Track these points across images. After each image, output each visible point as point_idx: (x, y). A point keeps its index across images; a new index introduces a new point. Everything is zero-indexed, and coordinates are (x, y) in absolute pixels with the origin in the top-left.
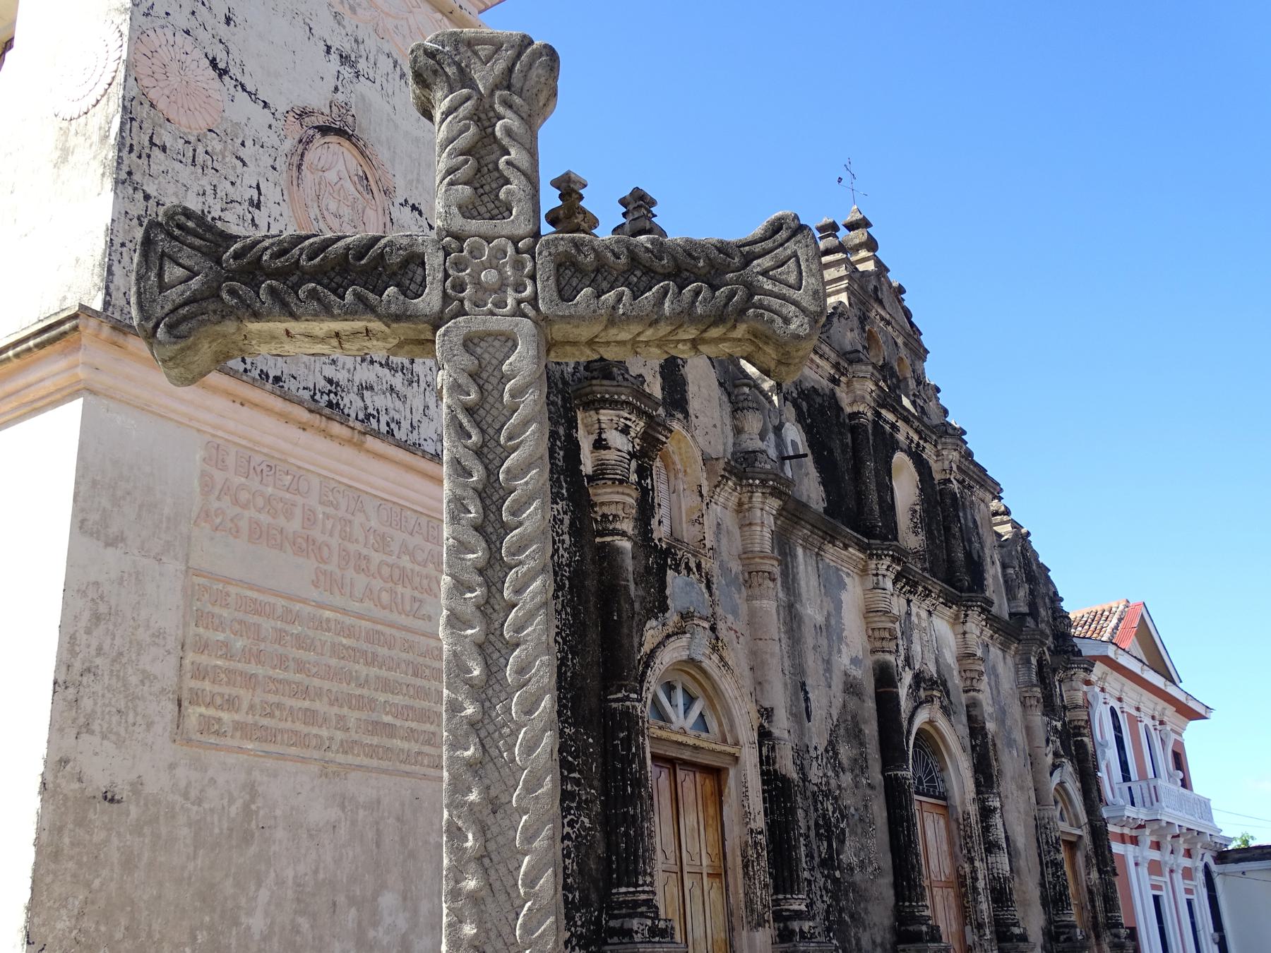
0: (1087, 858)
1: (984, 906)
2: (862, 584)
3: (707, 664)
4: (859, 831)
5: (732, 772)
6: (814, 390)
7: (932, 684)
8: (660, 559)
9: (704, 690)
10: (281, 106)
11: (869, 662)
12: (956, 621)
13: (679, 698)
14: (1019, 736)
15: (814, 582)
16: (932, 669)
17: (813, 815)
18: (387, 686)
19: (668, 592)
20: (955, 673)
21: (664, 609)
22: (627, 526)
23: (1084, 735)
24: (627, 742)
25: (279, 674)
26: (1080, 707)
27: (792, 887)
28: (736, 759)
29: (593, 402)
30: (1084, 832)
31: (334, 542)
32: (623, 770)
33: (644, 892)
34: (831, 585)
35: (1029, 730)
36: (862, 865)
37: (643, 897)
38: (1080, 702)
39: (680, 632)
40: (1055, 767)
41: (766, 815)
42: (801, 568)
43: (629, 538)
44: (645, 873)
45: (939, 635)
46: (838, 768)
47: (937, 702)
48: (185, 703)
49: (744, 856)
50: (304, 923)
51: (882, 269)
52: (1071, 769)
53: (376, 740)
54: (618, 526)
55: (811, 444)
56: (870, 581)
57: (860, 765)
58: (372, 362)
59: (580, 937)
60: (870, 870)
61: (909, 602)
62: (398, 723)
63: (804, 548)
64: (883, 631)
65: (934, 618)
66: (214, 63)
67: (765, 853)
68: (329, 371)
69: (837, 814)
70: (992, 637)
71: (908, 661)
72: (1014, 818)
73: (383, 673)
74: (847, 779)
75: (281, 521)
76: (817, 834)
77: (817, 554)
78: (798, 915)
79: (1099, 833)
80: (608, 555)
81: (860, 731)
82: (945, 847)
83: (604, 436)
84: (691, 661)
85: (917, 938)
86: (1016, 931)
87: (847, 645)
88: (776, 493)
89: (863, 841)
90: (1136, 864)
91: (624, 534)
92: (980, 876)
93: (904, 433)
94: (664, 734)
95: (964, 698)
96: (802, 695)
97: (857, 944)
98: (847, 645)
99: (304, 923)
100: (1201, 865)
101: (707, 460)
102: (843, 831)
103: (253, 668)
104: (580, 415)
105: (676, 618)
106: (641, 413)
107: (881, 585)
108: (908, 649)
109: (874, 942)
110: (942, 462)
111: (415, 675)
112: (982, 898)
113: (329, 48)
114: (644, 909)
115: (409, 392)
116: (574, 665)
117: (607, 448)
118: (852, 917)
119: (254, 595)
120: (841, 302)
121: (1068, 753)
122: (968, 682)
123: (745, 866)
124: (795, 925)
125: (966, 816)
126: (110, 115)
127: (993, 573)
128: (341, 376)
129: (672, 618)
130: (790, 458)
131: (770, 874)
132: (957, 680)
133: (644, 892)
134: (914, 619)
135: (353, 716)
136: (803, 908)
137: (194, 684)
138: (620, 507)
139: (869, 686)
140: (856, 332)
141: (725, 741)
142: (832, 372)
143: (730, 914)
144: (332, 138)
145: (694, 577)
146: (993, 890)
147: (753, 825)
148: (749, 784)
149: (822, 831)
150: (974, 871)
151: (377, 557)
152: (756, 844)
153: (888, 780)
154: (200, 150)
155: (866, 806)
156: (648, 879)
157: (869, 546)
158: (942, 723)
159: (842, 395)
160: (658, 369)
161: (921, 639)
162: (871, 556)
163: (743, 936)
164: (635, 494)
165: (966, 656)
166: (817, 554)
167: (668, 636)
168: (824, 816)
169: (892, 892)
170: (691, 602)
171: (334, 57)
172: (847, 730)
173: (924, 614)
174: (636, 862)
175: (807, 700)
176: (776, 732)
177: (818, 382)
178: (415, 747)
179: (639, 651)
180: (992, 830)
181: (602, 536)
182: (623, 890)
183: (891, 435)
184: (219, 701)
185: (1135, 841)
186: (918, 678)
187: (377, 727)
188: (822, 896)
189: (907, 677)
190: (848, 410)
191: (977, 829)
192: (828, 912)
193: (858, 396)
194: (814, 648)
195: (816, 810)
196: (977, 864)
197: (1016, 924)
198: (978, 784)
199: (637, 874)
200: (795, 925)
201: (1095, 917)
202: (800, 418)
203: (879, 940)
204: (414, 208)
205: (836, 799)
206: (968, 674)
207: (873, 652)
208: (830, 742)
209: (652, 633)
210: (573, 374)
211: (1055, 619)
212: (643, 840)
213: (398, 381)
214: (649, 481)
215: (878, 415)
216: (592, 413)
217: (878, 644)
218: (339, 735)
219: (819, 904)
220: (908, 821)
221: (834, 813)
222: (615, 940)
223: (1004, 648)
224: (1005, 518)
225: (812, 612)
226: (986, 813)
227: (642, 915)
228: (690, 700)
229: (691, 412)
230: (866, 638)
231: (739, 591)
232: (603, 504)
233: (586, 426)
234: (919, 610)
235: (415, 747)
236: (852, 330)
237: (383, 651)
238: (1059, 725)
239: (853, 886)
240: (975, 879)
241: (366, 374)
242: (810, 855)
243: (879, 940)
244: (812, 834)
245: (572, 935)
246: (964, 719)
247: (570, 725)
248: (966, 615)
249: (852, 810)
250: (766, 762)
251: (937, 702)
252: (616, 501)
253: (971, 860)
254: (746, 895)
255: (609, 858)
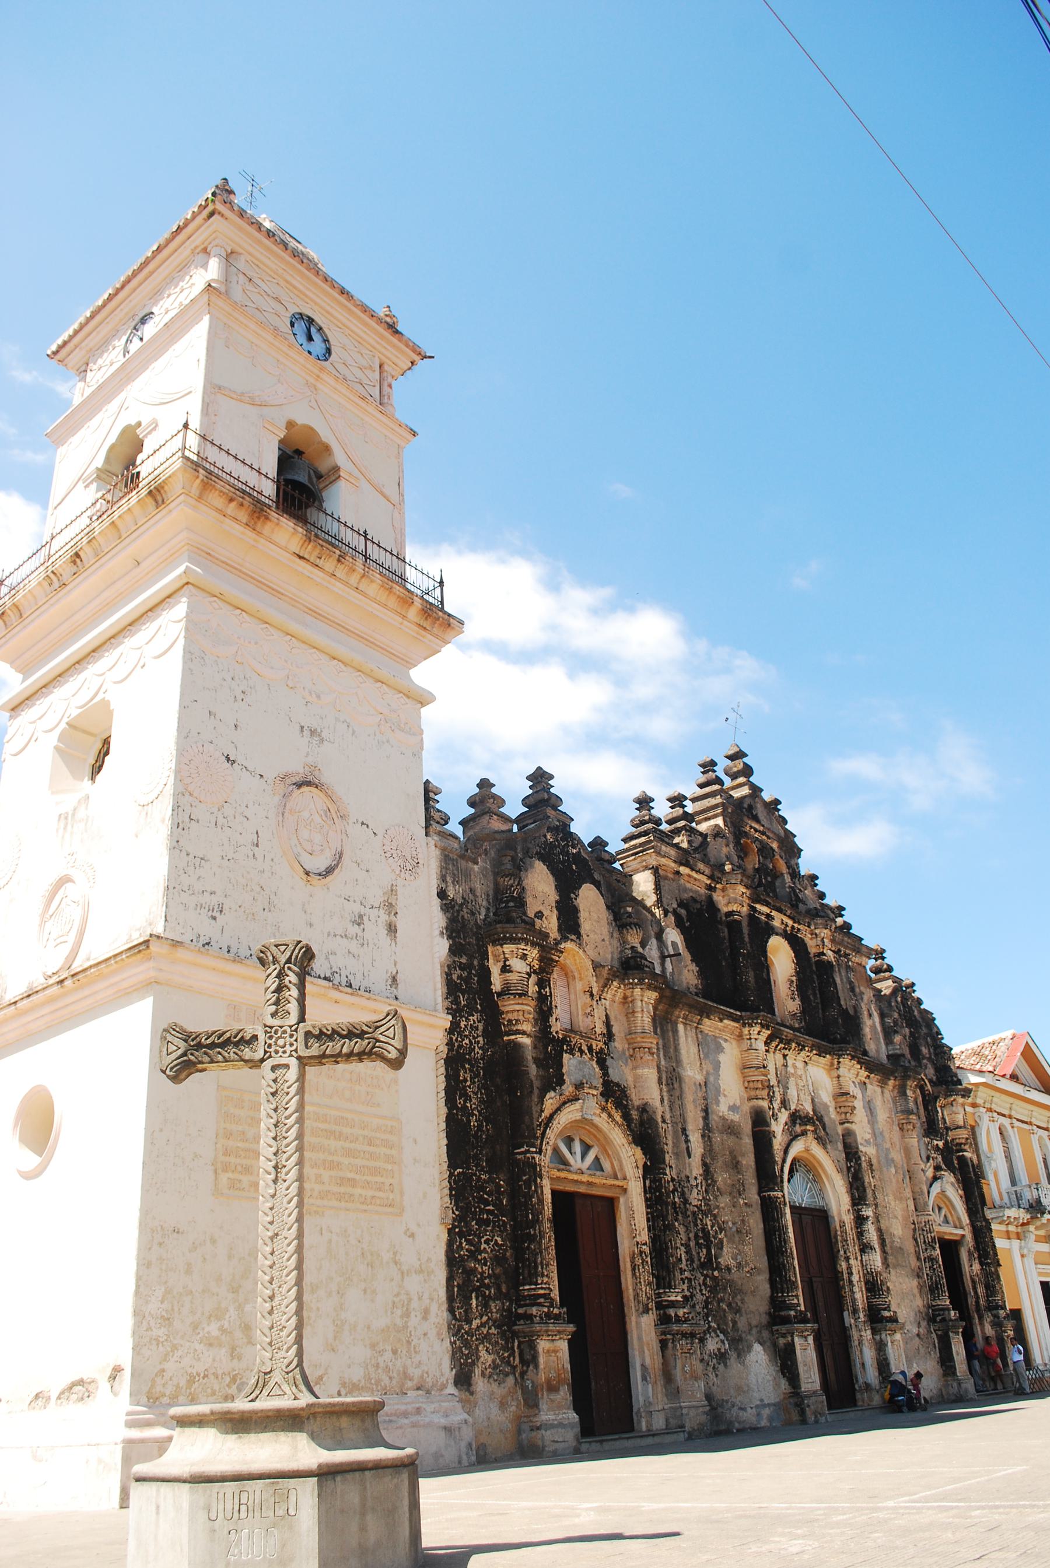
0: (969, 1251)
1: (858, 1296)
2: (739, 1047)
3: (597, 1120)
4: (737, 1239)
5: (622, 1200)
7: (806, 1120)
8: (553, 1048)
9: (598, 1140)
10: (270, 775)
11: (746, 1107)
13: (577, 1147)
14: (897, 1156)
15: (694, 1050)
17: (693, 1229)
18: (349, 1153)
19: (564, 1071)
20: (832, 1110)
21: (561, 1082)
22: (527, 1027)
23: (965, 1151)
24: (528, 1184)
26: (960, 1127)
27: (670, 1283)
29: (498, 940)
30: (967, 1233)
32: (526, 1204)
33: (542, 1288)
34: (709, 1048)
35: (907, 1151)
36: (739, 1266)
37: (542, 1292)
38: (961, 1123)
40: (935, 1178)
41: (649, 1230)
43: (529, 1036)
44: (543, 1275)
47: (810, 1135)
48: (219, 1171)
49: (632, 1261)
51: (756, 790)
52: (952, 1179)
53: (342, 1190)
54: (519, 1027)
55: (689, 945)
58: (335, 936)
61: (785, 1056)
62: (358, 1177)
63: (685, 1024)
65: (809, 1067)
67: (649, 1259)
69: (716, 1228)
70: (868, 1077)
71: (784, 1104)
73: (347, 1145)
76: (697, 1244)
77: (697, 1028)
78: (673, 1304)
81: (738, 1162)
83: (507, 963)
84: (584, 1120)
86: (886, 1314)
87: (725, 1096)
89: (740, 1247)
90: (1023, 1256)
91: (524, 1033)
93: (778, 920)
94: (562, 1174)
95: (840, 1130)
97: (879, 1508)
98: (725, 1096)
101: (596, 966)
102: (721, 1241)
104: (490, 949)
105: (571, 1089)
107: (754, 1047)
108: (784, 1094)
109: (750, 1324)
110: (819, 940)
111: (370, 1144)
112: (856, 1289)
113: (302, 728)
114: (542, 1300)
116: (488, 1130)
117: (510, 971)
118: (729, 1305)
120: (717, 826)
121: (950, 1168)
122: (843, 1116)
123: (633, 1269)
124: (672, 1312)
126: (164, 808)
127: (871, 1025)
129: (568, 1089)
130: (670, 956)
131: (653, 1274)
132: (833, 1115)
133: (542, 1288)
134: (790, 1069)
136: (679, 1298)
137: (227, 1159)
138: (521, 1013)
139: (747, 1128)
140: (731, 846)
141: (616, 1177)
142: (708, 882)
144: (305, 789)
145: (586, 1057)
147: (638, 1239)
148: (635, 1209)
149: (701, 1241)
150: (849, 1267)
152: (641, 1252)
153: (763, 1198)
154: (220, 818)
155: (743, 1221)
156: (545, 1279)
158: (817, 1151)
159: (718, 898)
160: (554, 905)
161: (797, 1085)
162: (744, 1025)
164: (533, 1003)
165: (842, 1095)
166: (697, 1028)
167: (565, 1103)
168: (703, 1230)
169: (768, 1286)
170: (584, 1076)
171: (306, 732)
173: (800, 1065)
174: (536, 1267)
177: (697, 892)
178: (370, 1193)
179: (541, 1116)
180: (866, 1234)
181: (508, 1035)
182: (527, 1287)
183: (767, 923)
184: (239, 1168)
186: (796, 1118)
187: (342, 1181)
188: (701, 1290)
190: (725, 909)
192: (707, 1302)
193: (733, 899)
196: (852, 1262)
197: (888, 1309)
198: (853, 1199)
199: (536, 1275)
200: (672, 1312)
202: (679, 924)
206: (843, 1109)
207: (750, 1099)
209: (551, 1101)
210: (484, 920)
211: (936, 1055)
212: (541, 1252)
213: (354, 946)
214: (547, 989)
215: (754, 909)
216: (499, 947)
217: (753, 1093)
219: (699, 1296)
220: (779, 1230)
221: (712, 1227)
222: (522, 1322)
223: (883, 1084)
224: (887, 974)
225: (692, 1072)
227: (540, 1305)
228: (586, 1148)
229: (582, 932)
230: (743, 1089)
231: (626, 1064)
232: (508, 1012)
233: (495, 956)
234: (796, 1060)
235: (370, 1193)
237: (346, 1130)
238: (941, 1144)
239: (732, 1283)
240: (850, 1274)
244: (692, 1244)
245: (489, 1319)
246: (840, 1146)
247: (485, 1172)
248: (839, 1062)
249: (730, 1224)
251: (810, 1135)
252: (520, 1014)
254: (634, 1290)
255: (517, 1265)
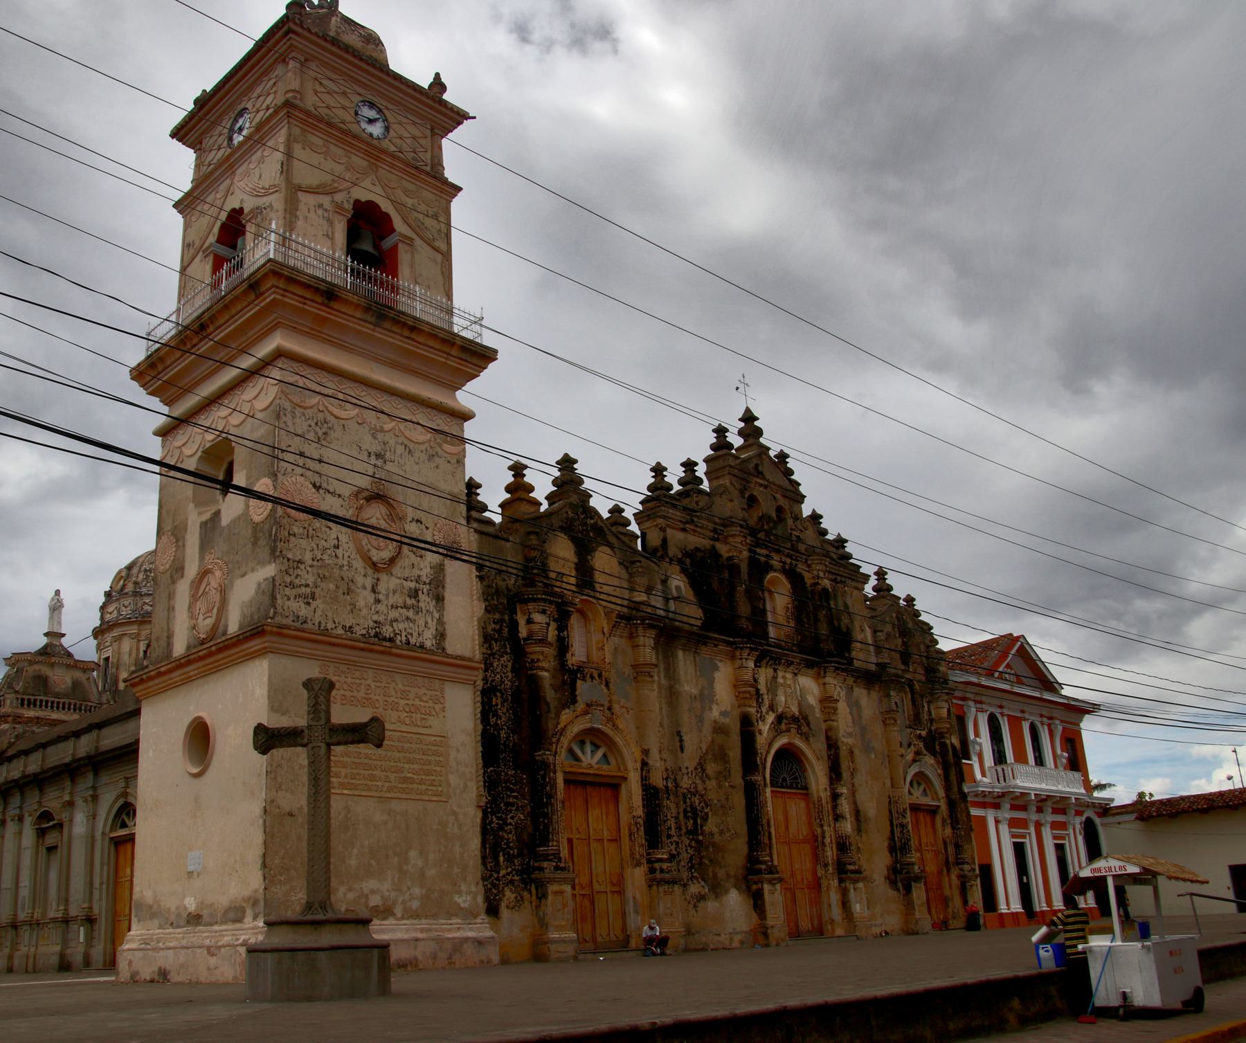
0: (944, 821)
1: (829, 853)
6: (697, 549)
7: (794, 719)
8: (569, 677)
11: (736, 713)
12: (817, 677)
16: (795, 710)
17: (682, 806)
18: (410, 761)
19: (577, 693)
21: (574, 701)
24: (544, 777)
25: (357, 760)
28: (625, 779)
30: (943, 804)
31: (381, 698)
34: (707, 673)
36: (721, 832)
39: (586, 713)
42: (681, 663)
45: (802, 688)
46: (704, 777)
50: (374, 863)
56: (738, 663)
57: (724, 775)
59: (517, 871)
60: (728, 835)
64: (748, 692)
66: (314, 485)
68: (375, 617)
71: (772, 708)
72: (868, 792)
74: (712, 784)
75: (355, 693)
79: (957, 801)
80: (534, 682)
81: (726, 755)
82: (804, 818)
85: (759, 872)
86: (851, 867)
88: (651, 626)
92: (827, 835)
95: (823, 726)
96: (677, 738)
99: (374, 863)
100: (1078, 822)
102: (707, 814)
103: (345, 759)
106: (551, 602)
110: (817, 574)
112: (828, 849)
115: (417, 618)
118: (711, 861)
119: (247, 362)
121: (932, 752)
125: (820, 799)
127: (863, 634)
128: (381, 618)
129: (580, 706)
135: (392, 776)
139: (735, 728)
140: (736, 502)
143: (622, 860)
146: (838, 844)
150: (823, 832)
151: (403, 702)
157: (734, 643)
159: (723, 549)
162: (736, 648)
163: (628, 872)
165: (828, 702)
172: (714, 755)
175: (681, 741)
176: (650, 762)
183: (766, 562)
185: (997, 806)
186: (780, 719)
189: (771, 718)
191: (827, 807)
192: (691, 859)
193: (735, 548)
194: (689, 710)
195: (685, 802)
196: (825, 828)
200: (657, 866)
201: (947, 859)
203: (732, 873)
204: (418, 521)
205: (702, 796)
208: (700, 764)
213: (411, 614)
218: (387, 785)
226: (835, 797)
236: (731, 501)
239: (714, 844)
240: (824, 837)
241: (394, 614)
242: (679, 828)
243: (732, 873)
244: (681, 816)
246: (823, 738)
250: (644, 779)
253: (822, 826)
